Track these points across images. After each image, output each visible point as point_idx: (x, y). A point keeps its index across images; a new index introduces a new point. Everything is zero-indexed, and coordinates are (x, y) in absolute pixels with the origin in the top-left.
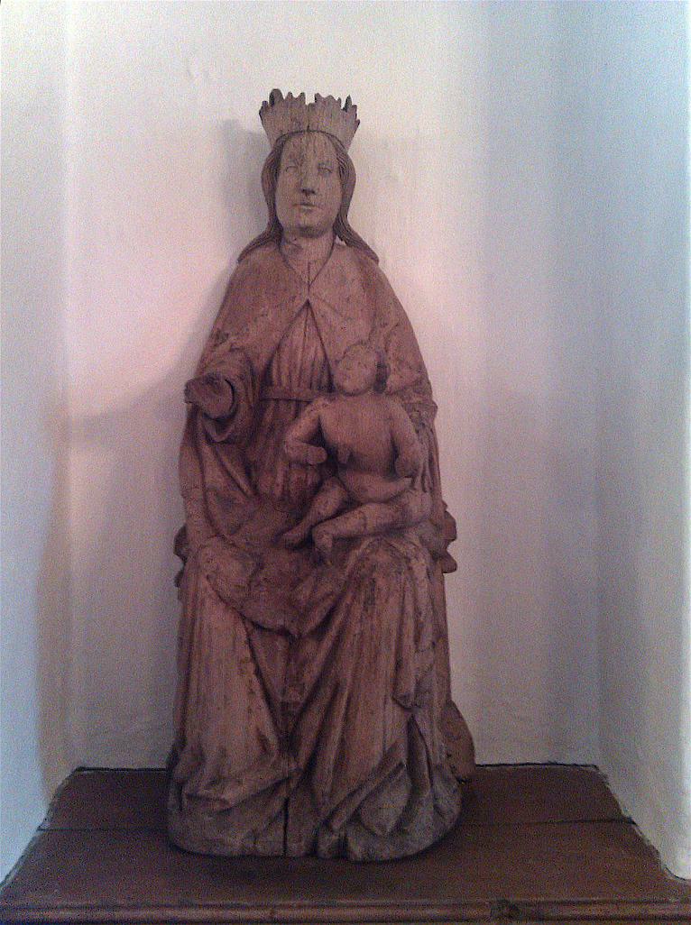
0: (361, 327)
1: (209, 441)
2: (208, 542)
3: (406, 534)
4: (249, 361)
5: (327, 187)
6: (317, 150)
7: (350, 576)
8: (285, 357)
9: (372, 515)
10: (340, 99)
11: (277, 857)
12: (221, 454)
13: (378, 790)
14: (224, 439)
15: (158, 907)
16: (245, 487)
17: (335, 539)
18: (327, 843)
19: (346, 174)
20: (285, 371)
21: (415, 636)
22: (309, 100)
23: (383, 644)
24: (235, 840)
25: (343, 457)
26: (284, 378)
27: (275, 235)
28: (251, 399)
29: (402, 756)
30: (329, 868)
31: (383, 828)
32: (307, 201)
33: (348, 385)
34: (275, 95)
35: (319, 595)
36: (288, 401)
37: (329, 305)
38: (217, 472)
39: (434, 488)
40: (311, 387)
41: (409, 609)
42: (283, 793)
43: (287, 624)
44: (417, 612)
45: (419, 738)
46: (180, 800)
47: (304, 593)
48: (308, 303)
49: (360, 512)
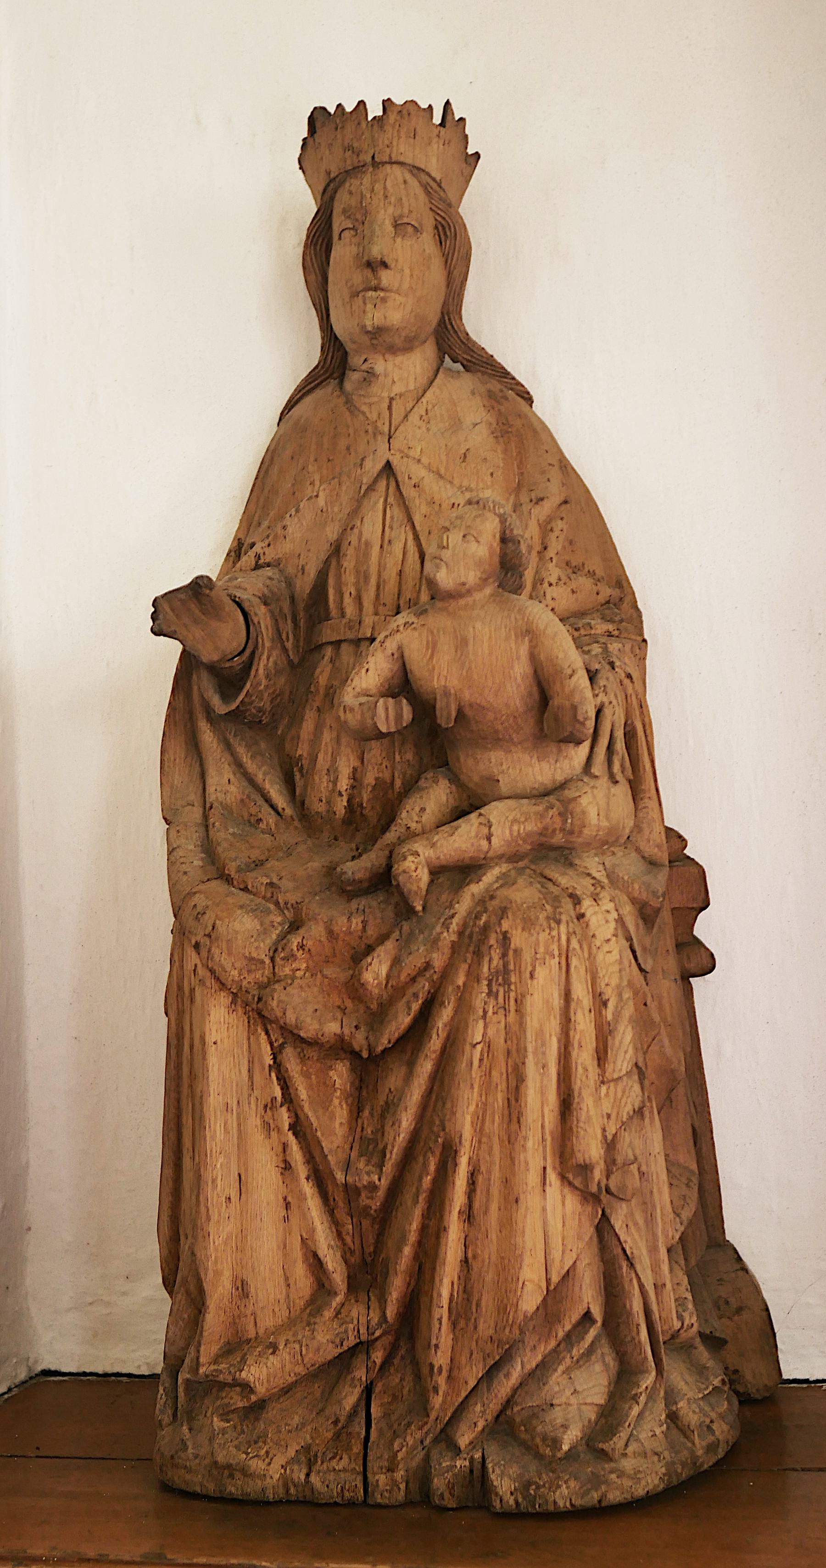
2: (202, 887)
3: (577, 861)
4: (289, 583)
6: (393, 195)
7: (461, 934)
8: (349, 563)
9: (504, 824)
13: (544, 1368)
14: (233, 706)
16: (281, 801)
17: (437, 872)
18: (447, 1471)
22: (375, 110)
24: (272, 1468)
25: (445, 717)
27: (335, 364)
28: (289, 645)
29: (588, 1296)
31: (556, 1443)
32: (374, 283)
33: (444, 578)
37: (429, 468)
38: (228, 773)
43: (347, 1031)
45: (624, 1264)
47: (376, 971)
48: (388, 464)
49: (480, 815)
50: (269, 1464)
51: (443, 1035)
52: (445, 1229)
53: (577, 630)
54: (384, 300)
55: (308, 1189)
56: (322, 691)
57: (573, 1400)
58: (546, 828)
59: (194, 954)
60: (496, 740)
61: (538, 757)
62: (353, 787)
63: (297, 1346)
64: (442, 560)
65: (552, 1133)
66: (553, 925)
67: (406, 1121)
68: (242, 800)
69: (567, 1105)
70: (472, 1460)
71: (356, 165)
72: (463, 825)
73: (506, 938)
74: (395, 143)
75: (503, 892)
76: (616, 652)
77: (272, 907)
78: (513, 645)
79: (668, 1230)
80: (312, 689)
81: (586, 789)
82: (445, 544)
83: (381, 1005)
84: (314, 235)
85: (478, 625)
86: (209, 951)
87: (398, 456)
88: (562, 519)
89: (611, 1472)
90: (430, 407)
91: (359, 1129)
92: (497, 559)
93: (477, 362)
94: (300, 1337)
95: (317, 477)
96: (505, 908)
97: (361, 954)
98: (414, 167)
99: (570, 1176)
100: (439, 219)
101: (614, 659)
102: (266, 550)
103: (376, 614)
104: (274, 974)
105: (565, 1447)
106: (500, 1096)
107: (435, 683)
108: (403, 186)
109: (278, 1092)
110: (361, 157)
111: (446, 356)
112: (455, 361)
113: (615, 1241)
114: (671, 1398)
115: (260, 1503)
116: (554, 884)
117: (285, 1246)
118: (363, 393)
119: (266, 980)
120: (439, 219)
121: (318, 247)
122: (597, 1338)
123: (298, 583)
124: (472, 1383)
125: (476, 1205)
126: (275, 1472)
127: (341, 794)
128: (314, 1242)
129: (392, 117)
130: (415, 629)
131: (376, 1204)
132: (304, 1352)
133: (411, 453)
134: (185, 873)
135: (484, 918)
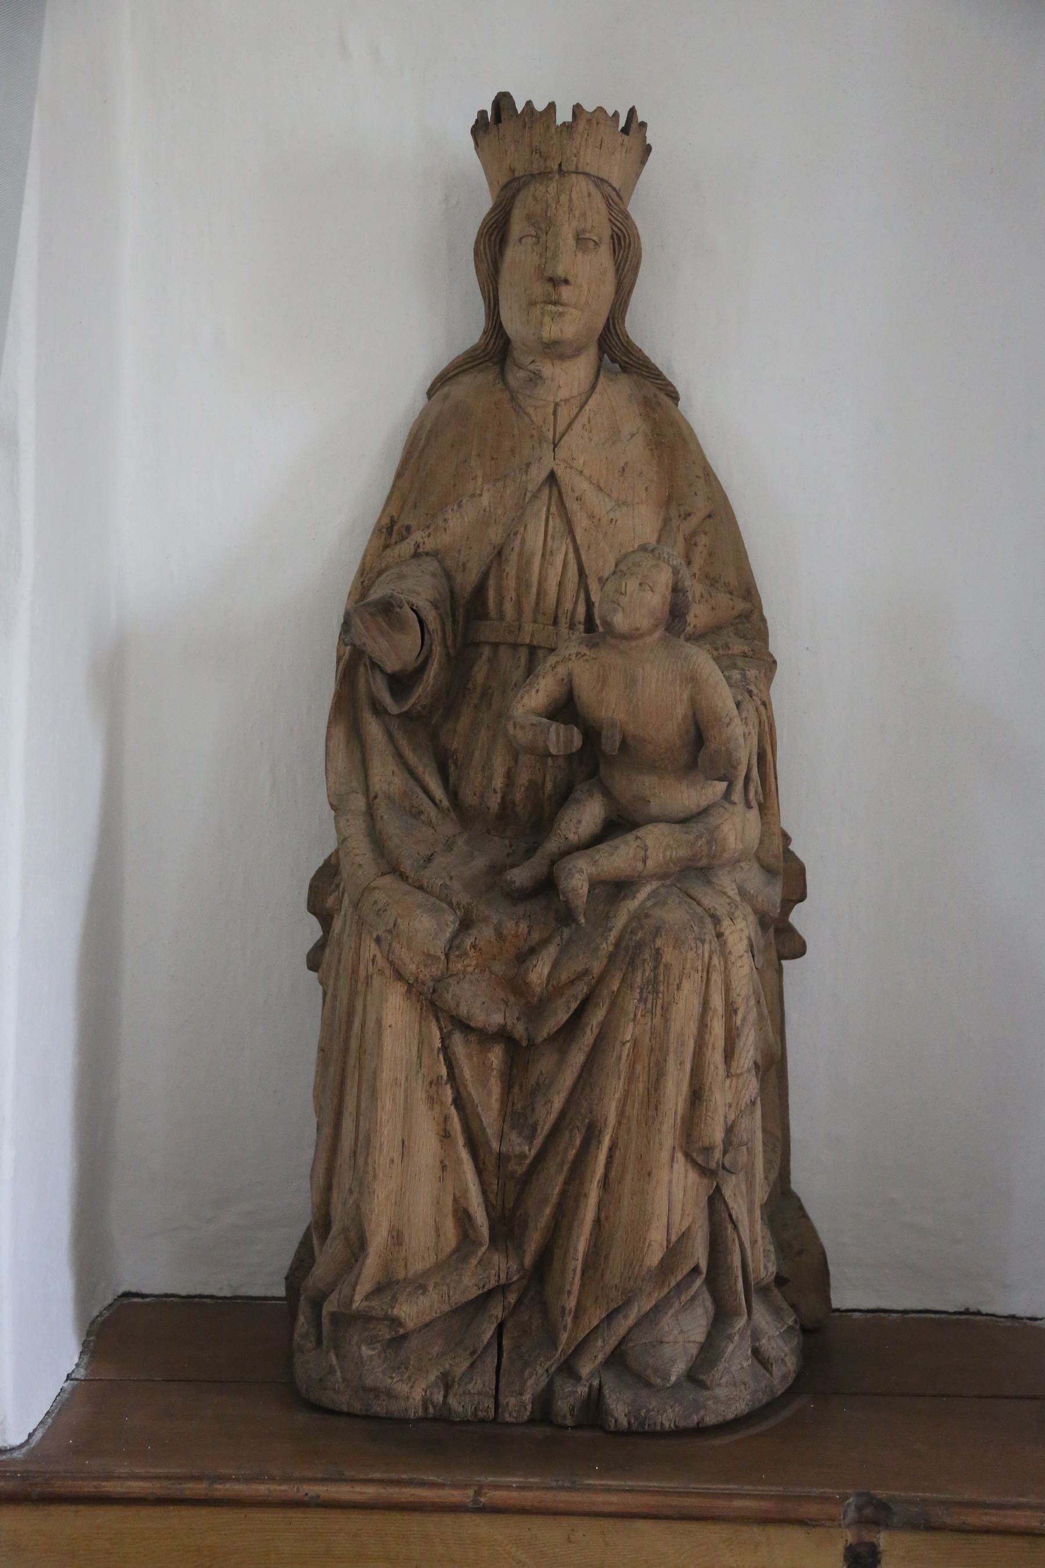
0: (641, 523)
1: (378, 710)
3: (714, 880)
5: (589, 273)
6: (579, 206)
7: (617, 945)
8: (511, 569)
9: (655, 846)
10: (616, 114)
11: (482, 1421)
12: (398, 735)
13: (658, 1309)
14: (405, 708)
15: (285, 1479)
16: (439, 793)
18: (569, 1398)
19: (624, 248)
21: (725, 1051)
22: (564, 115)
23: (671, 1057)
24: (414, 1392)
25: (610, 744)
26: (509, 608)
27: (494, 352)
28: (449, 642)
29: (699, 1254)
30: (577, 1438)
31: (666, 1377)
32: (554, 298)
33: (620, 621)
34: (503, 102)
35: (564, 977)
36: (515, 646)
37: (589, 479)
38: (391, 765)
39: (766, 805)
40: (555, 622)
41: (717, 1001)
42: (497, 1311)
43: (509, 1022)
44: (731, 1010)
45: (730, 1226)
46: (319, 1326)
47: (539, 971)
49: (637, 838)
50: (412, 1387)
51: (596, 1031)
52: (585, 1195)
53: (716, 649)
54: (561, 315)
55: (464, 1155)
56: (479, 689)
57: (680, 1338)
58: (695, 855)
59: (373, 945)
60: (653, 767)
62: (507, 785)
63: (445, 1288)
65: (682, 1118)
66: (699, 944)
67: (558, 1102)
68: (405, 793)
69: (697, 1095)
70: (591, 1387)
72: (622, 847)
73: (658, 954)
74: (582, 153)
75: (658, 912)
76: (753, 679)
77: (445, 906)
79: (761, 1194)
80: (470, 686)
81: (727, 815)
82: (623, 590)
83: (540, 1000)
86: (390, 945)
87: (563, 466)
88: (705, 533)
89: (709, 1399)
91: (510, 1104)
92: (667, 608)
94: (448, 1281)
95: (480, 473)
96: (660, 928)
97: (525, 955)
98: (598, 178)
99: (695, 1155)
101: (752, 687)
102: (426, 540)
103: (535, 621)
104: (447, 968)
105: (673, 1379)
106: (641, 1086)
108: (587, 200)
109: (444, 1072)
111: (606, 356)
113: (723, 1207)
114: (756, 1336)
115: (401, 1421)
116: (698, 904)
117: (438, 1203)
119: (439, 973)
121: (493, 238)
122: (700, 1287)
123: (459, 578)
124: (595, 1323)
125: (613, 1174)
126: (418, 1395)
127: (495, 792)
128: (466, 1199)
129: (582, 125)
130: (587, 660)
131: (520, 1170)
132: (451, 1293)
134: (360, 866)
135: (640, 934)
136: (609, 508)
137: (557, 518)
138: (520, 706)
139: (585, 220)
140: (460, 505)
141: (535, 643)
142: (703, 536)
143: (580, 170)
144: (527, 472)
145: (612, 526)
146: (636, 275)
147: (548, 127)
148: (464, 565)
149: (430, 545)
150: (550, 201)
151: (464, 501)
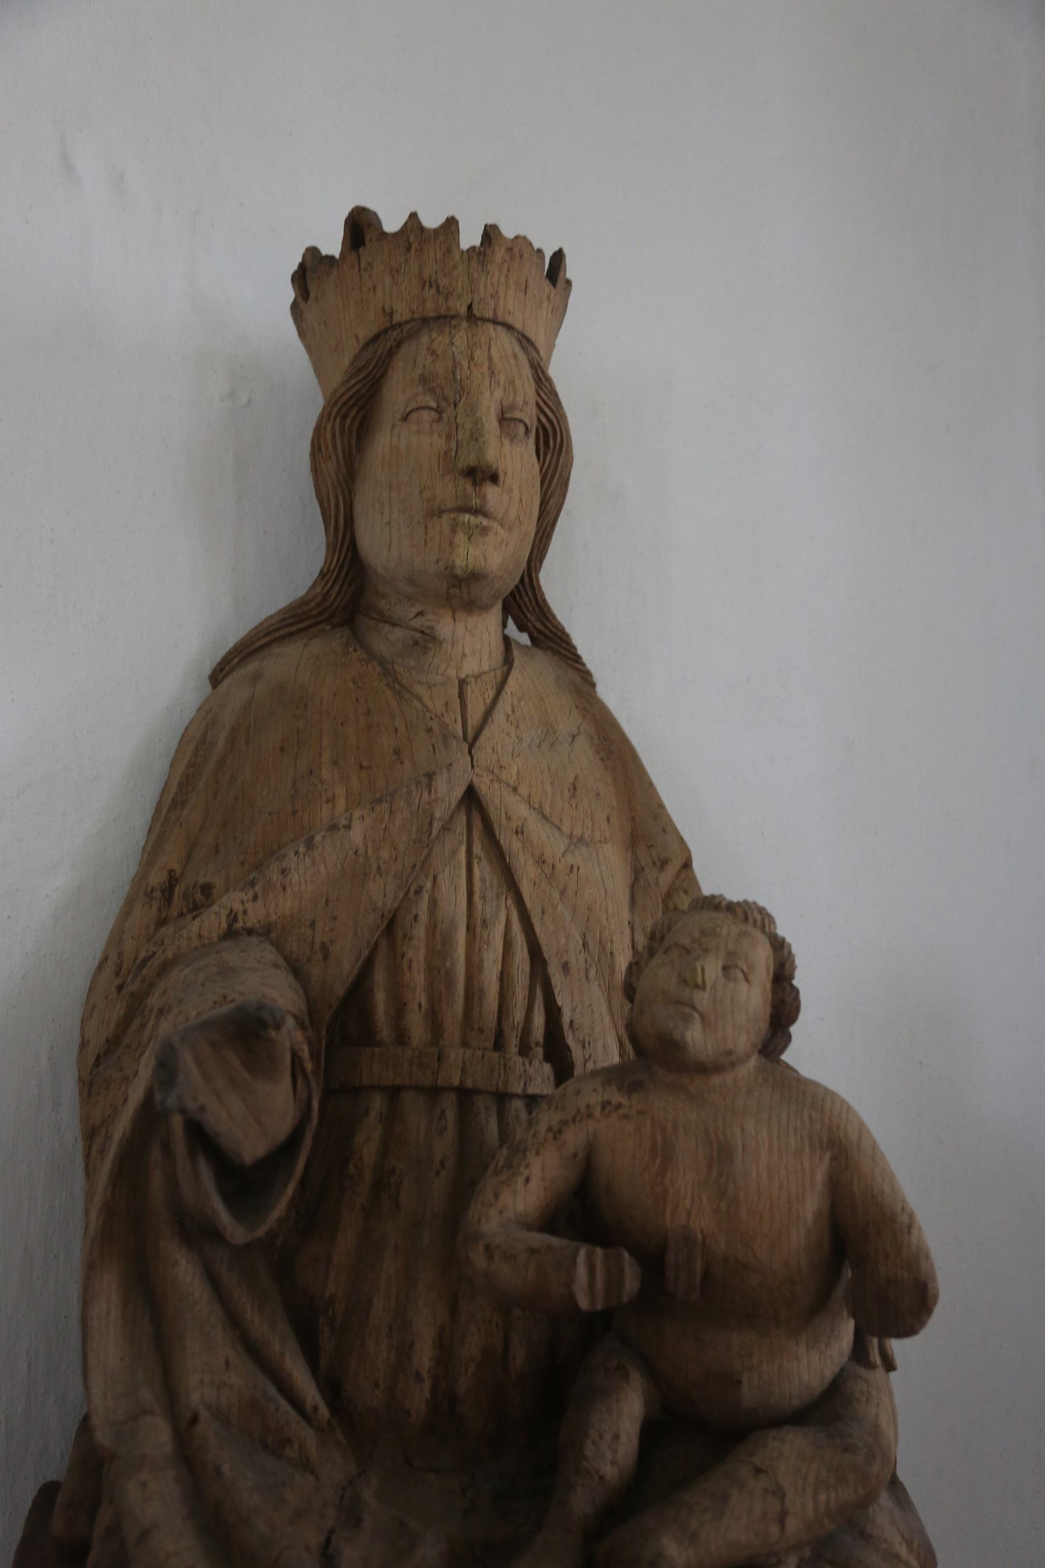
1: (198, 1233)
8: (417, 953)
14: (261, 1232)
20: (418, 997)
22: (470, 238)
26: (416, 1025)
27: (344, 599)
32: (475, 502)
36: (433, 1093)
37: (528, 801)
40: (499, 1044)
49: (758, 1471)
54: (484, 531)
61: (807, 1343)
64: (694, 1008)
71: (442, 311)
78: (807, 1165)
80: (352, 1169)
82: (700, 982)
84: (345, 403)
85: (750, 1124)
90: (515, 702)
93: (550, 635)
95: (341, 793)
100: (543, 420)
103: (465, 1044)
107: (668, 1218)
108: (513, 362)
110: (451, 303)
112: (521, 628)
118: (412, 663)
120: (543, 420)
121: (348, 422)
127: (419, 1378)
129: (499, 254)
130: (626, 1117)
133: (503, 776)
136: (562, 849)
137: (485, 863)
138: (493, 1212)
139: (515, 391)
140: (310, 844)
141: (469, 1084)
142: (683, 896)
143: (500, 318)
144: (429, 786)
145: (573, 876)
146: (564, 495)
147: (449, 251)
148: (324, 948)
149: (255, 914)
150: (458, 357)
151: (318, 838)
